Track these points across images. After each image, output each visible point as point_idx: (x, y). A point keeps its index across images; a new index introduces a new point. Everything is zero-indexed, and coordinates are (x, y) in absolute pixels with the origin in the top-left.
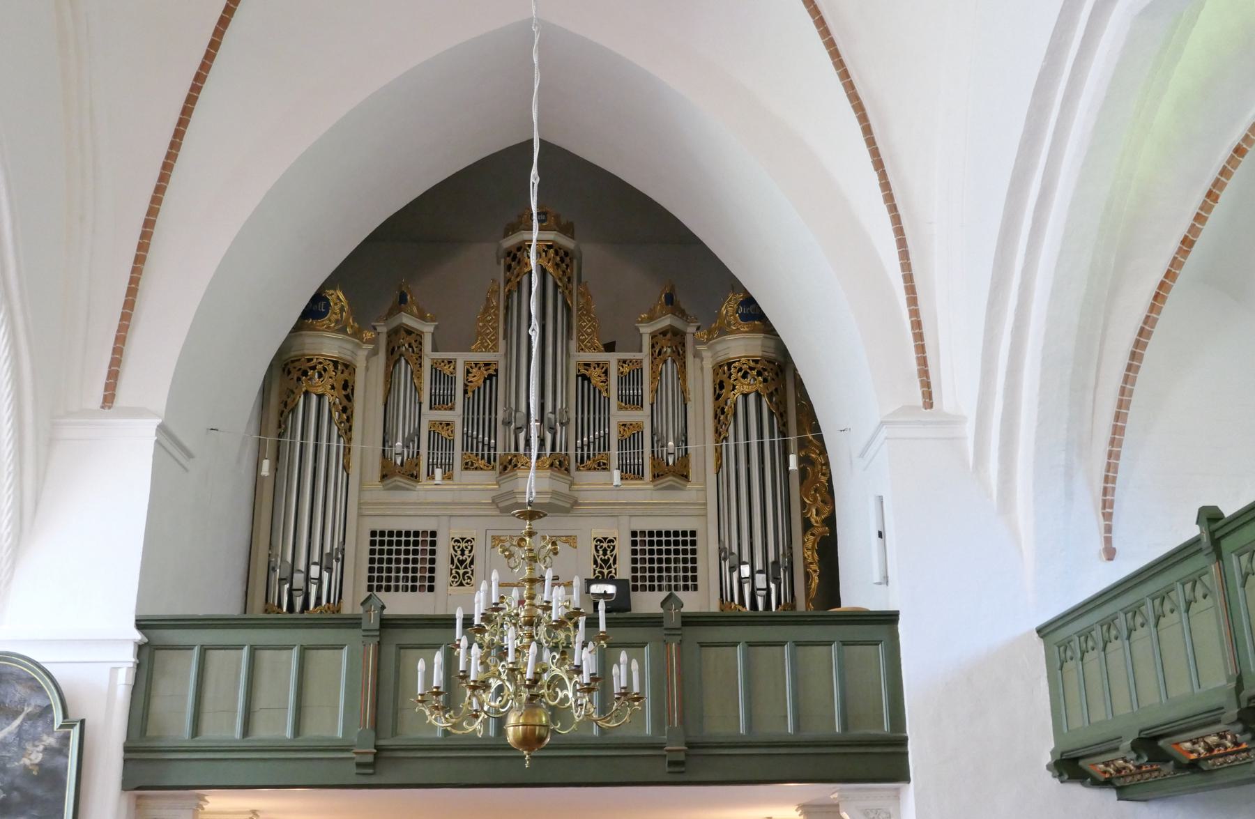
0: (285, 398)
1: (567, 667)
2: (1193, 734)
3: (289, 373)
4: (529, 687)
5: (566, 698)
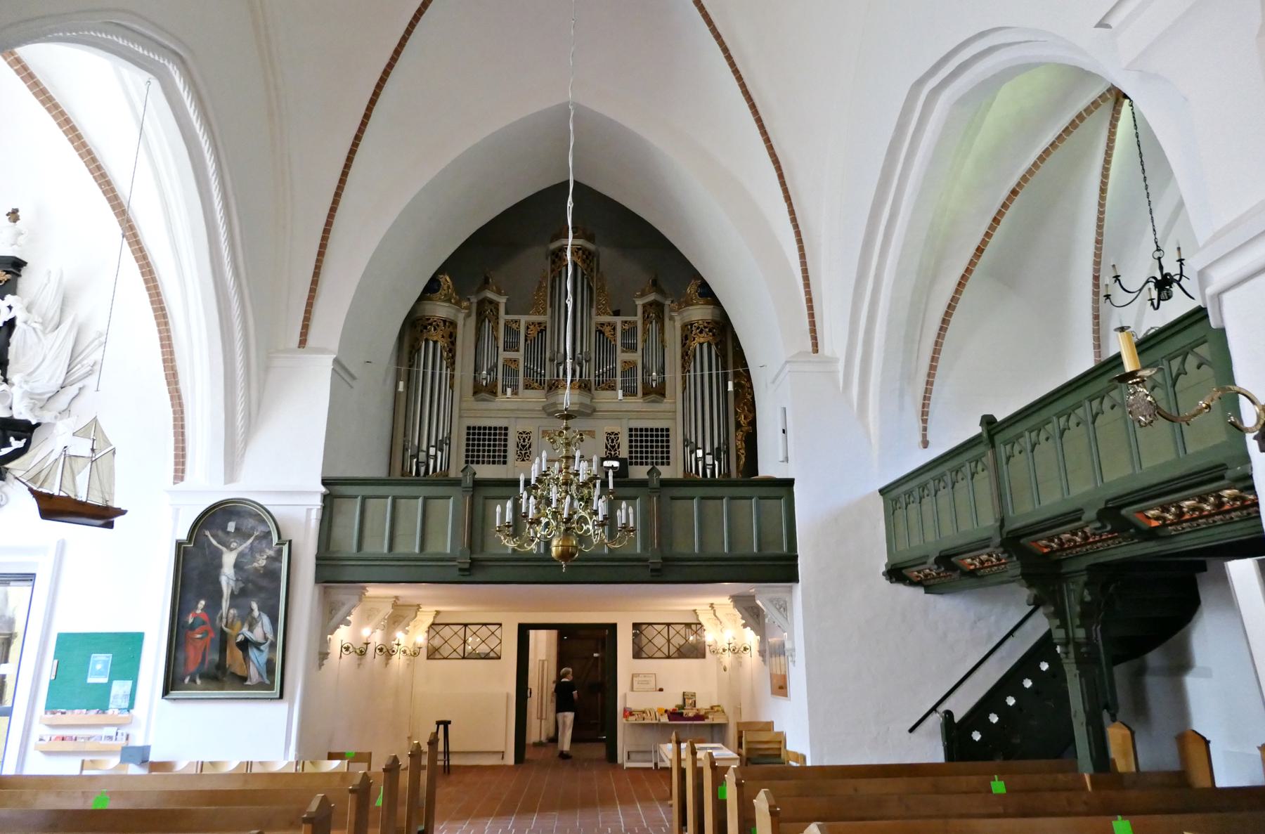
1: (589, 511)
2: (972, 554)
4: (565, 523)
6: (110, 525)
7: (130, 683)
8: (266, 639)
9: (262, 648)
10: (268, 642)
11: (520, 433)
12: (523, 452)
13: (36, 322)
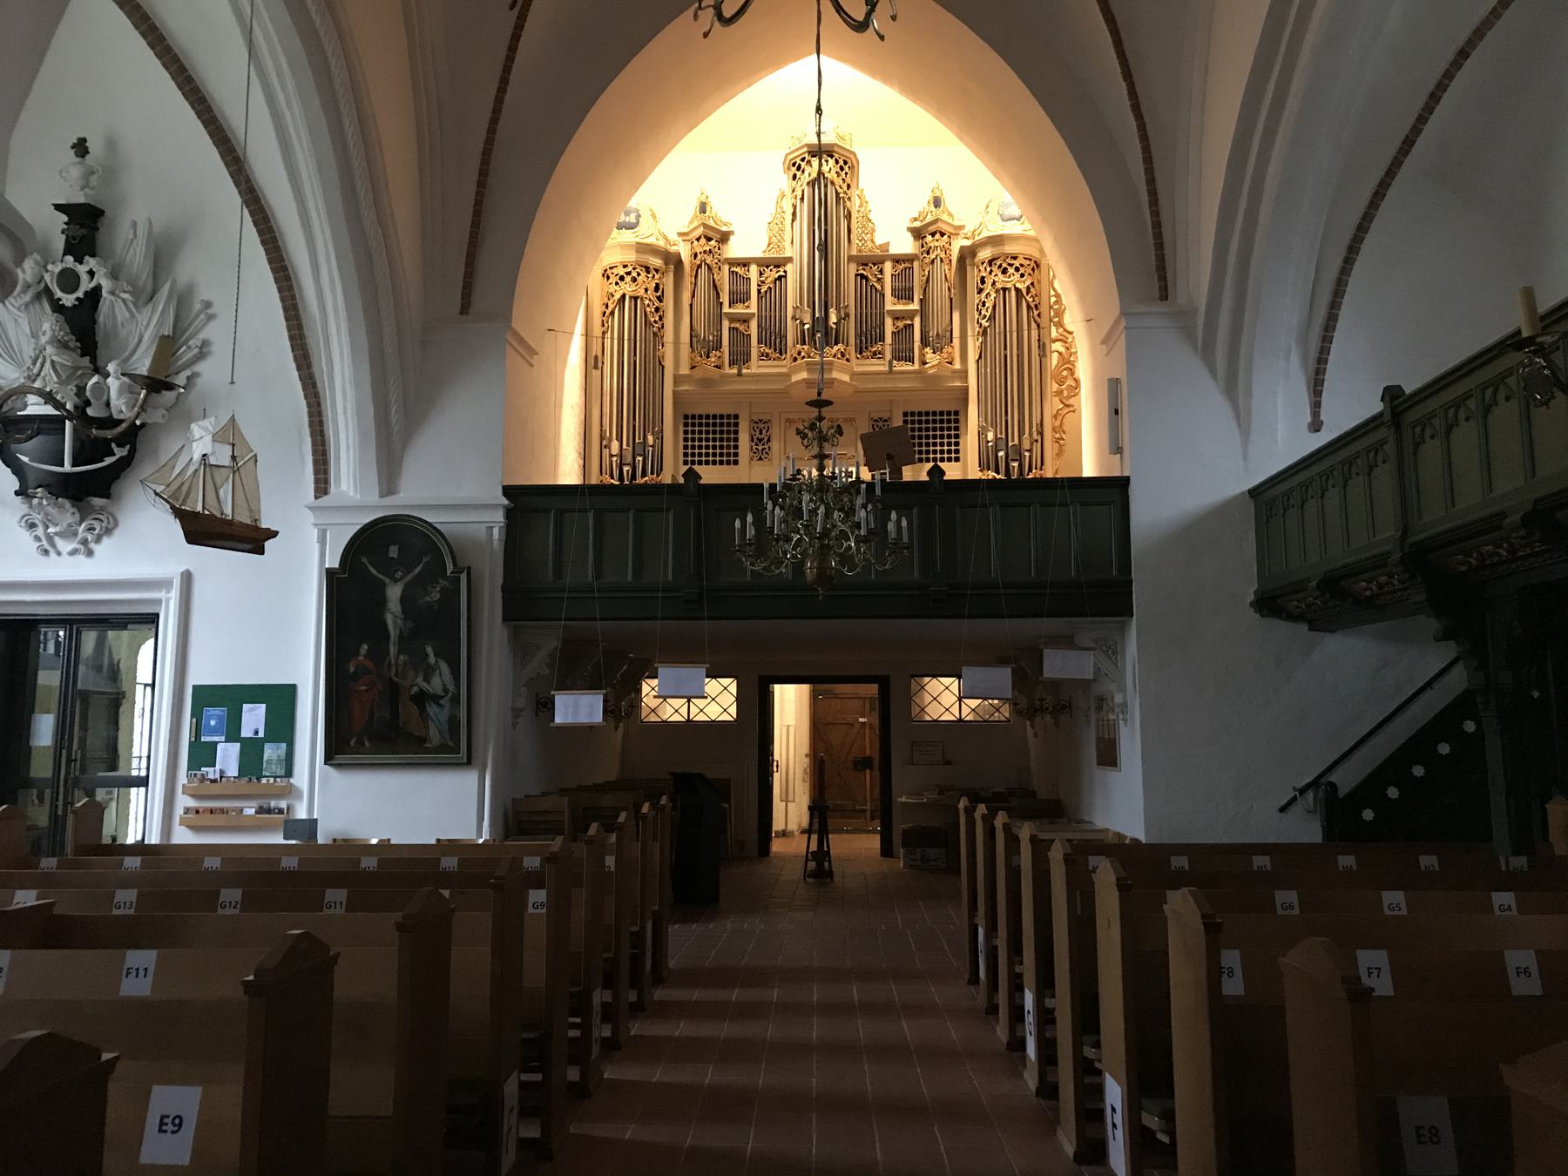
0: (606, 301)
1: (850, 523)
2: (1367, 576)
3: (608, 278)
4: (819, 538)
5: (850, 546)
6: (260, 551)
7: (284, 745)
8: (446, 691)
9: (442, 702)
10: (450, 694)
11: (756, 422)
12: (760, 448)
13: (124, 292)
